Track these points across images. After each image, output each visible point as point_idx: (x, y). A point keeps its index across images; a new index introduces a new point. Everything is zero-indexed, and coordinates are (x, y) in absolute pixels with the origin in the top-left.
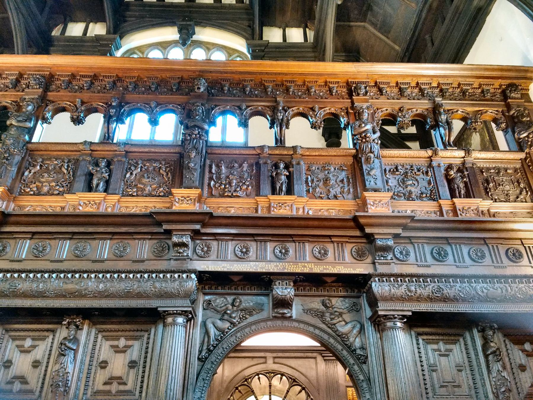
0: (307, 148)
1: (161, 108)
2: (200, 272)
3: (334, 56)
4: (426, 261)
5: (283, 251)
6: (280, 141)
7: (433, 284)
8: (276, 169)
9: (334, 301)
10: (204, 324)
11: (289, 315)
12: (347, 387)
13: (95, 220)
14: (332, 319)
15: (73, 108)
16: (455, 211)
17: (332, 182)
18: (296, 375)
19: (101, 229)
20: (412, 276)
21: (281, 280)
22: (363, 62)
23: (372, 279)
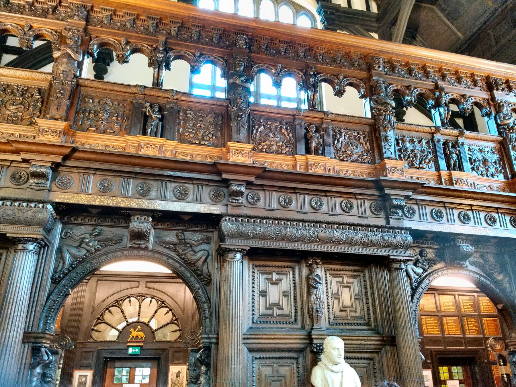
0: (336, 114)
1: (204, 58)
2: (57, 203)
3: (404, 39)
4: (336, 211)
5: (288, 201)
6: (157, 83)
7: (362, 232)
8: (310, 131)
10: (60, 251)
11: (144, 246)
12: (422, 315)
13: (333, 181)
14: (490, 270)
15: (20, 31)
16: (451, 181)
18: (164, 298)
19: (335, 189)
20: (351, 225)
21: (140, 215)
22: (415, 45)
23: (224, 219)
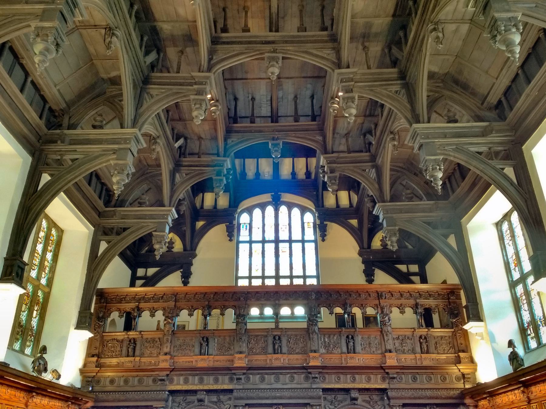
9: (374, 396)
17: (372, 345)
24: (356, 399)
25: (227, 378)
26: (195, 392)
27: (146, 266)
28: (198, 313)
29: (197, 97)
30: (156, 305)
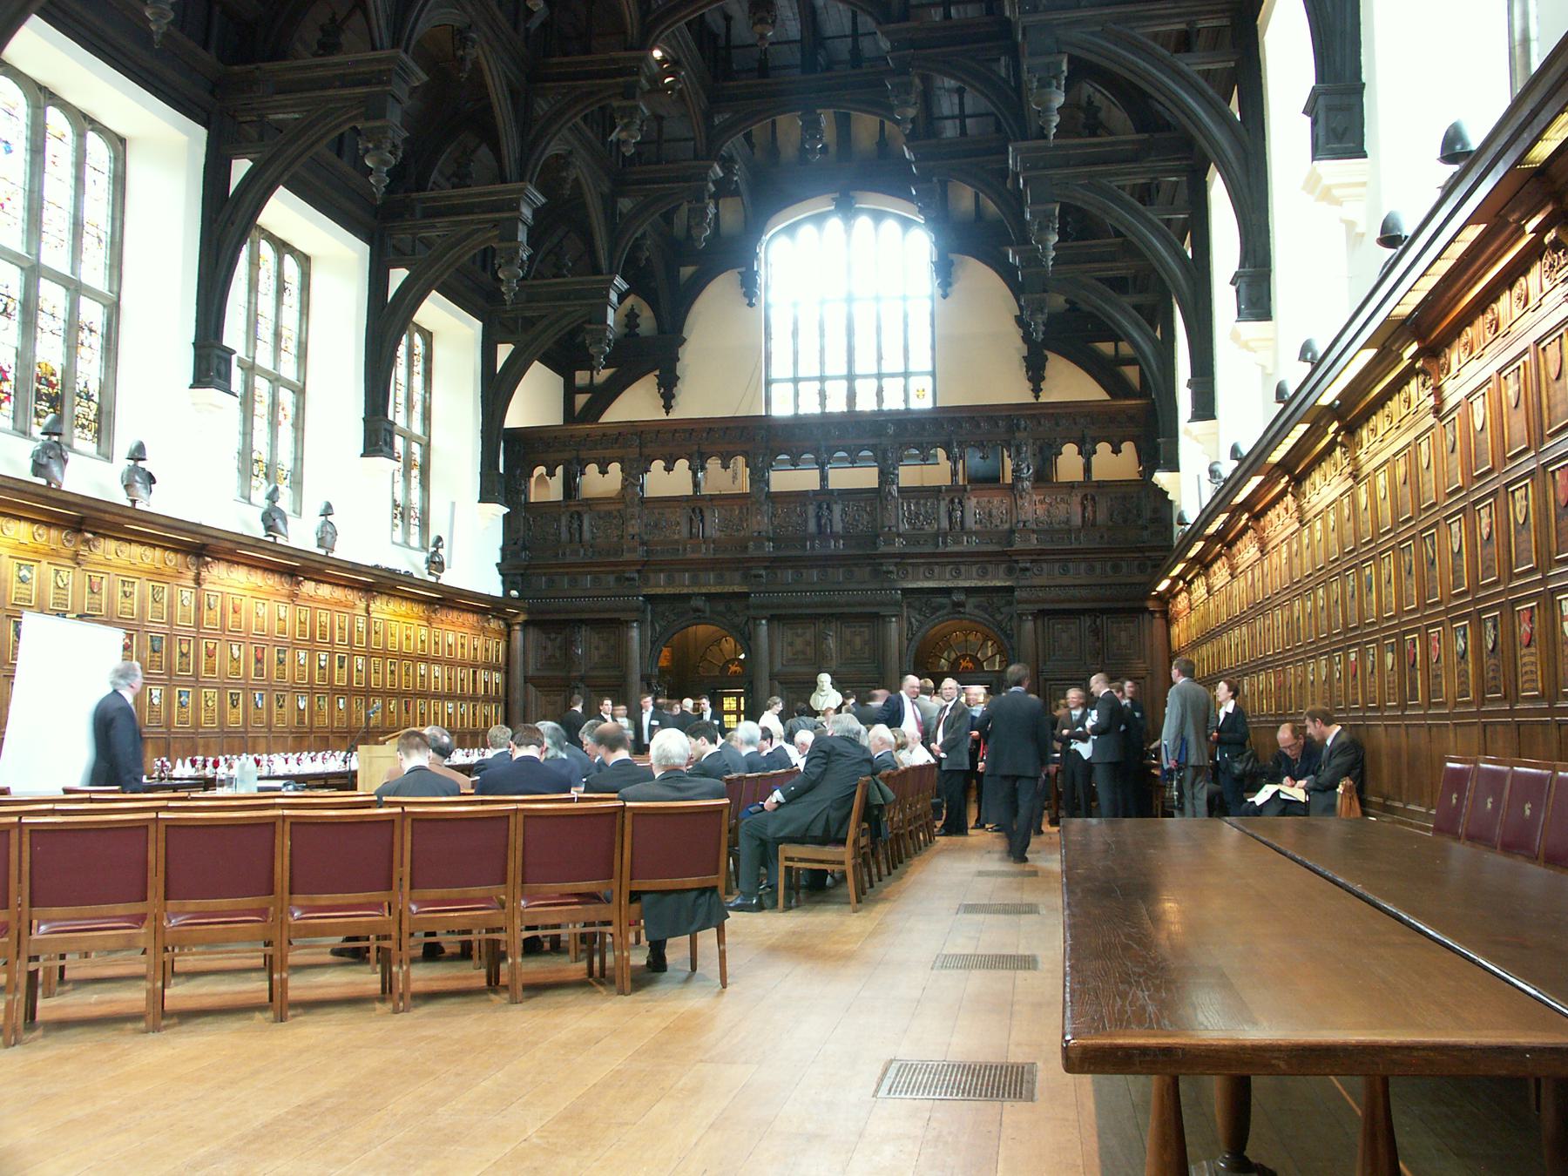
24: (962, 605)
25: (737, 576)
26: (688, 597)
27: (589, 364)
28: (682, 465)
29: (625, 103)
30: (608, 453)
